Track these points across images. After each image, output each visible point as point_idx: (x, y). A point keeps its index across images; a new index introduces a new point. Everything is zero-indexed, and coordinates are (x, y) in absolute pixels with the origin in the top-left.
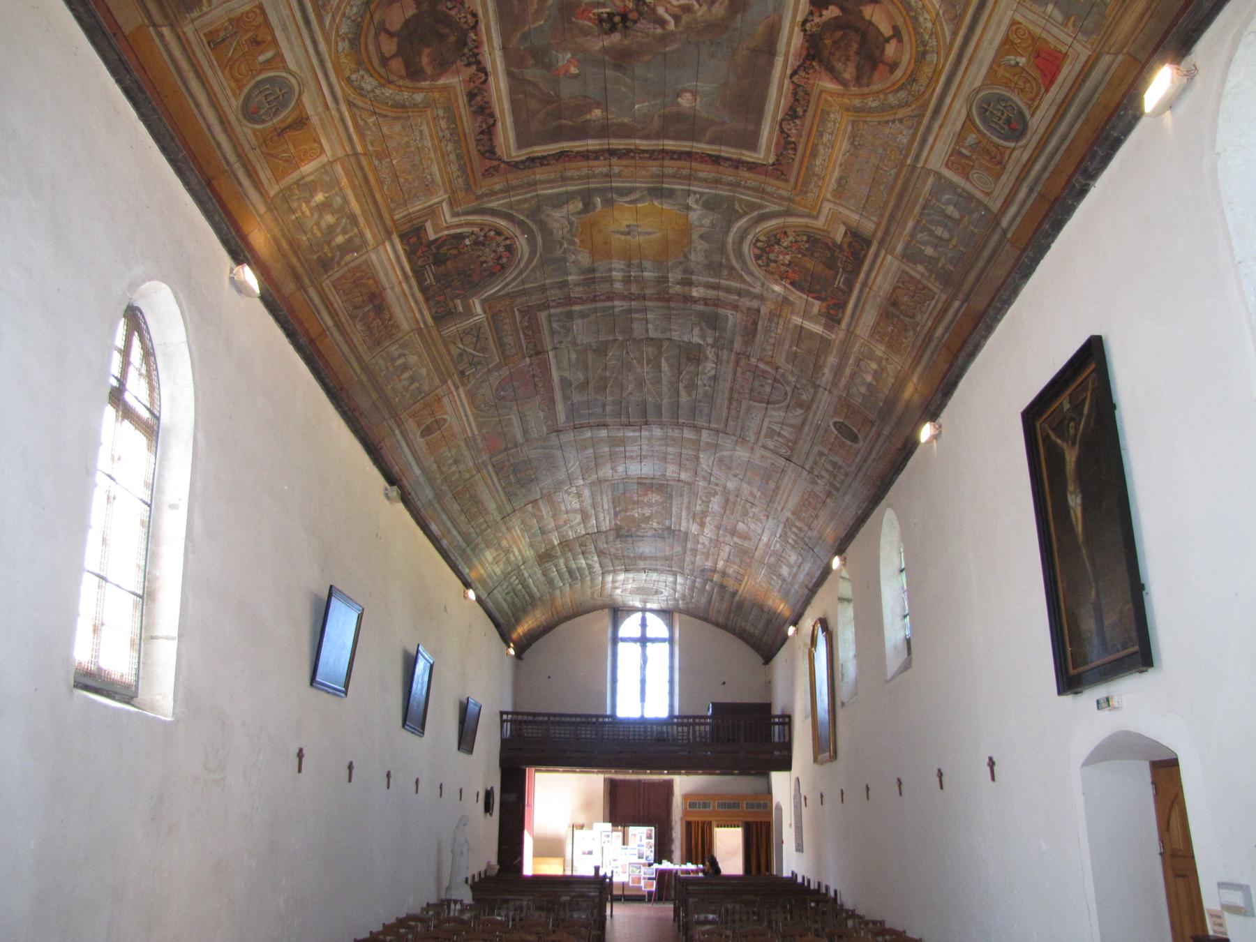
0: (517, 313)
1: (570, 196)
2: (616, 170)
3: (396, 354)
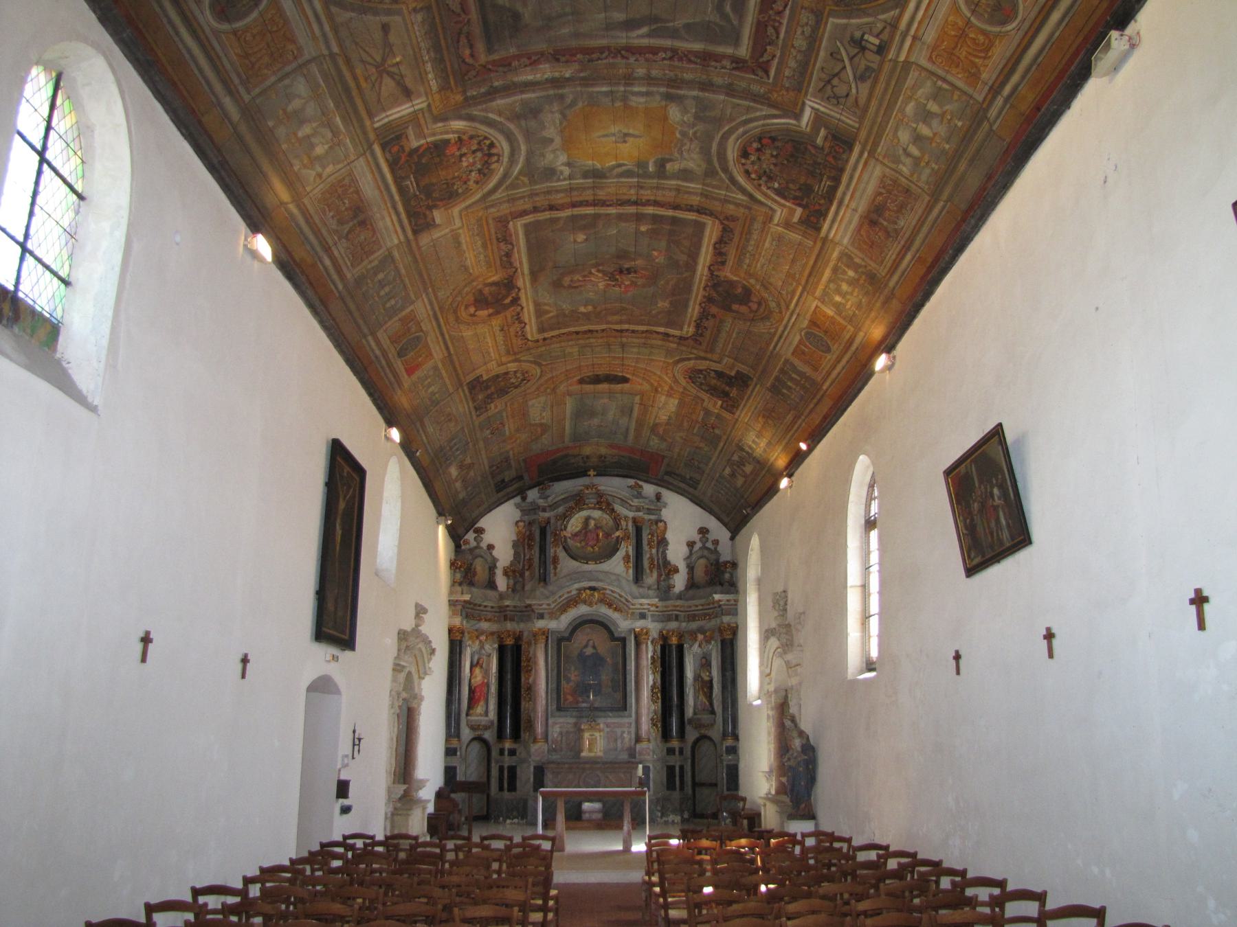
0: (772, 73)
1: (675, 176)
2: (633, 191)
3: (908, 161)
